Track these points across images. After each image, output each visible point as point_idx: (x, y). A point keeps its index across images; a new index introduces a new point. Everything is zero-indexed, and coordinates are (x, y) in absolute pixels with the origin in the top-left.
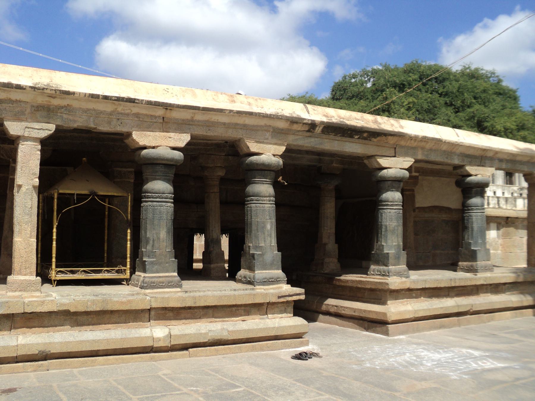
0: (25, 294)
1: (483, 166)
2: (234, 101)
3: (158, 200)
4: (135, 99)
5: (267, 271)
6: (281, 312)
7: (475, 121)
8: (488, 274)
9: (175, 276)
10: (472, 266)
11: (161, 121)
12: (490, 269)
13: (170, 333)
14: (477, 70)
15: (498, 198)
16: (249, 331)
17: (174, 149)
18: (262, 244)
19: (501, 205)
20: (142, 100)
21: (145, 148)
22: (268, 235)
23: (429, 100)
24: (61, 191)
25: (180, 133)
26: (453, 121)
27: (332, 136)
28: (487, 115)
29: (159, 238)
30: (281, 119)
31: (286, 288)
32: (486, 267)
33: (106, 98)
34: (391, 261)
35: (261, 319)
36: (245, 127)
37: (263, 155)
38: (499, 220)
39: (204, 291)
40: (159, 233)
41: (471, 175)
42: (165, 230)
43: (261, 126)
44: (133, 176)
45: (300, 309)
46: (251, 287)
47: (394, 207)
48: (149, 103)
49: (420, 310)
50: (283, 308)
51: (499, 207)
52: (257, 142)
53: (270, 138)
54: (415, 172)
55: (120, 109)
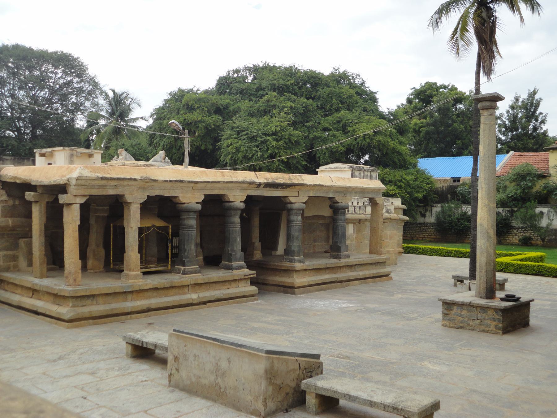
0: (136, 281)
2: (224, 176)
7: (341, 125)
8: (347, 260)
10: (338, 255)
12: (348, 257)
14: (344, 72)
15: (355, 207)
16: (232, 294)
17: (197, 203)
18: (235, 249)
19: (356, 211)
21: (184, 203)
23: (304, 105)
26: (323, 124)
27: (268, 189)
28: (350, 121)
29: (191, 249)
31: (246, 271)
34: (295, 254)
38: (355, 221)
40: (192, 248)
45: (253, 282)
46: (231, 271)
51: (355, 213)
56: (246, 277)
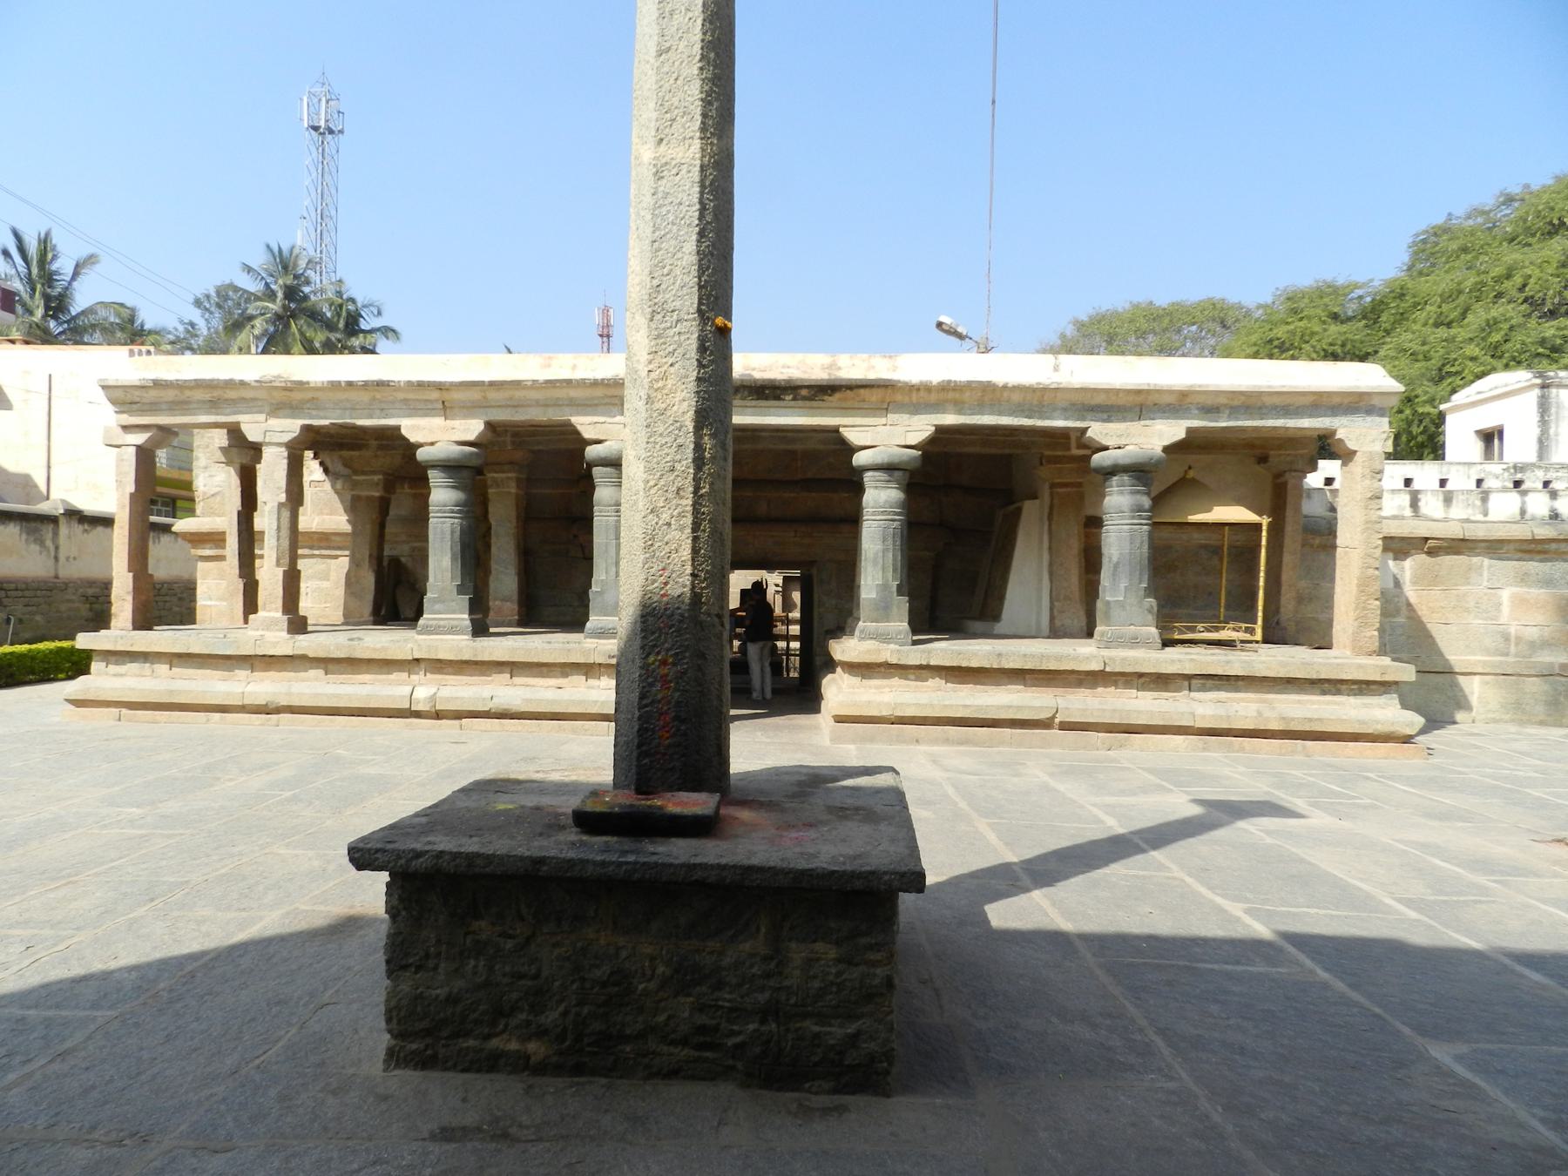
21: (421, 445)
41: (1106, 448)
44: (513, 484)
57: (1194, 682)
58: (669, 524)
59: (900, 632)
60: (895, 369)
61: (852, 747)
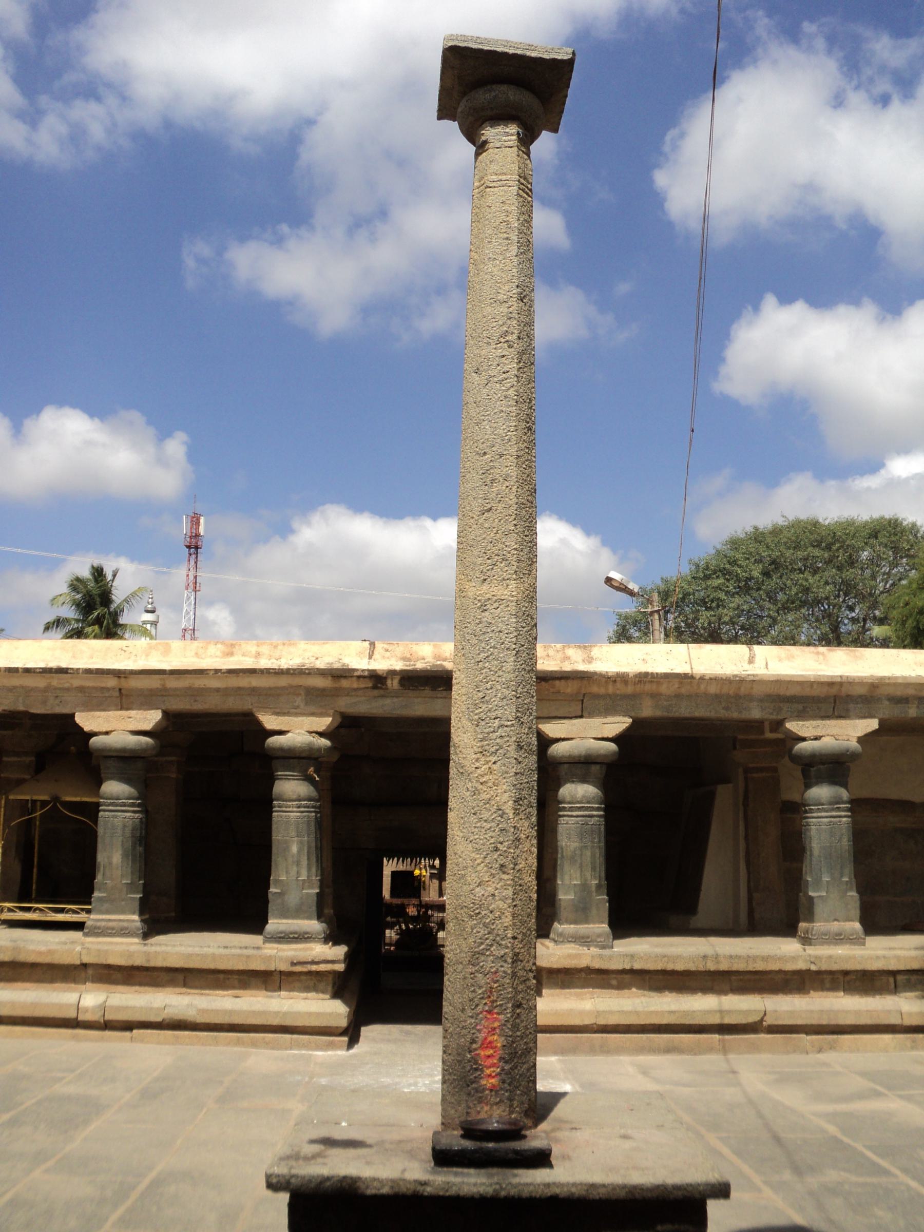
1: (840, 717)
3: (111, 808)
4: (67, 669)
5: (290, 921)
6: (307, 989)
9: (134, 921)
11: (117, 694)
13: (105, 1002)
20: (78, 669)
22: (293, 862)
24: (11, 797)
25: (145, 710)
29: (110, 864)
30: (309, 674)
32: (841, 934)
33: (27, 671)
35: (267, 997)
36: (253, 691)
37: (289, 735)
39: (174, 946)
41: (804, 739)
42: (120, 852)
43: (283, 688)
47: (575, 813)
48: (89, 671)
49: (611, 1012)
50: (311, 984)
52: (277, 714)
53: (302, 705)
54: (771, 731)
55: (55, 683)
56: (298, 969)
57: (525, 407)
58: (493, 895)
59: (599, 936)
60: (590, 660)
61: (553, 1059)
